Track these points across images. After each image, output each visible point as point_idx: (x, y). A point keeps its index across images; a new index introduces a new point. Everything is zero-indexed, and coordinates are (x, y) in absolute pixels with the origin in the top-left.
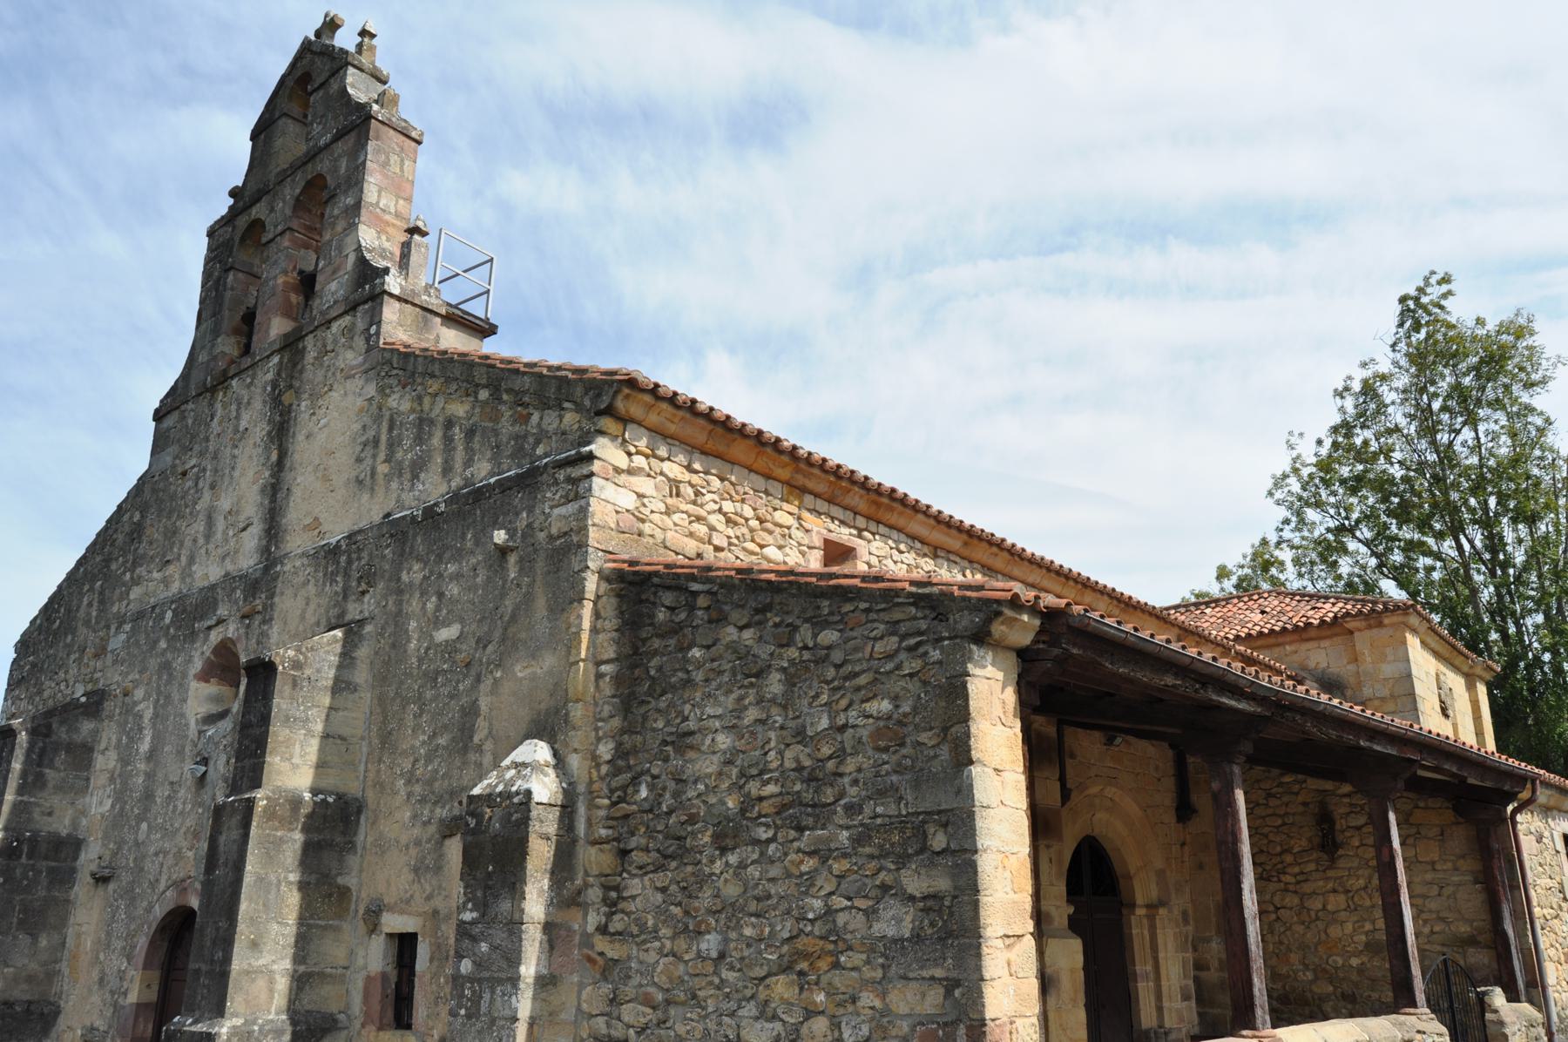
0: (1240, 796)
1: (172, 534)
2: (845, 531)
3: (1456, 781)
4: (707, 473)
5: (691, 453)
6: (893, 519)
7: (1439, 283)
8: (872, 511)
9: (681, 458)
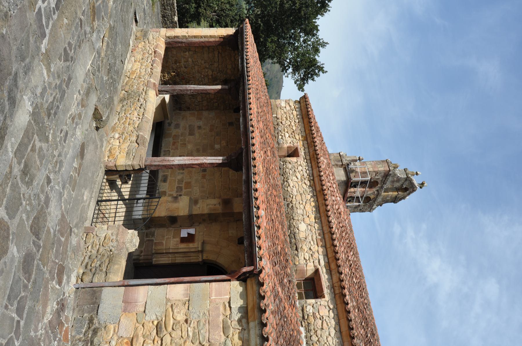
0: (219, 87)
2: (303, 154)
3: (346, 302)
4: (298, 119)
5: (300, 115)
6: (313, 163)
7: (39, 206)
8: (312, 156)
9: (298, 113)
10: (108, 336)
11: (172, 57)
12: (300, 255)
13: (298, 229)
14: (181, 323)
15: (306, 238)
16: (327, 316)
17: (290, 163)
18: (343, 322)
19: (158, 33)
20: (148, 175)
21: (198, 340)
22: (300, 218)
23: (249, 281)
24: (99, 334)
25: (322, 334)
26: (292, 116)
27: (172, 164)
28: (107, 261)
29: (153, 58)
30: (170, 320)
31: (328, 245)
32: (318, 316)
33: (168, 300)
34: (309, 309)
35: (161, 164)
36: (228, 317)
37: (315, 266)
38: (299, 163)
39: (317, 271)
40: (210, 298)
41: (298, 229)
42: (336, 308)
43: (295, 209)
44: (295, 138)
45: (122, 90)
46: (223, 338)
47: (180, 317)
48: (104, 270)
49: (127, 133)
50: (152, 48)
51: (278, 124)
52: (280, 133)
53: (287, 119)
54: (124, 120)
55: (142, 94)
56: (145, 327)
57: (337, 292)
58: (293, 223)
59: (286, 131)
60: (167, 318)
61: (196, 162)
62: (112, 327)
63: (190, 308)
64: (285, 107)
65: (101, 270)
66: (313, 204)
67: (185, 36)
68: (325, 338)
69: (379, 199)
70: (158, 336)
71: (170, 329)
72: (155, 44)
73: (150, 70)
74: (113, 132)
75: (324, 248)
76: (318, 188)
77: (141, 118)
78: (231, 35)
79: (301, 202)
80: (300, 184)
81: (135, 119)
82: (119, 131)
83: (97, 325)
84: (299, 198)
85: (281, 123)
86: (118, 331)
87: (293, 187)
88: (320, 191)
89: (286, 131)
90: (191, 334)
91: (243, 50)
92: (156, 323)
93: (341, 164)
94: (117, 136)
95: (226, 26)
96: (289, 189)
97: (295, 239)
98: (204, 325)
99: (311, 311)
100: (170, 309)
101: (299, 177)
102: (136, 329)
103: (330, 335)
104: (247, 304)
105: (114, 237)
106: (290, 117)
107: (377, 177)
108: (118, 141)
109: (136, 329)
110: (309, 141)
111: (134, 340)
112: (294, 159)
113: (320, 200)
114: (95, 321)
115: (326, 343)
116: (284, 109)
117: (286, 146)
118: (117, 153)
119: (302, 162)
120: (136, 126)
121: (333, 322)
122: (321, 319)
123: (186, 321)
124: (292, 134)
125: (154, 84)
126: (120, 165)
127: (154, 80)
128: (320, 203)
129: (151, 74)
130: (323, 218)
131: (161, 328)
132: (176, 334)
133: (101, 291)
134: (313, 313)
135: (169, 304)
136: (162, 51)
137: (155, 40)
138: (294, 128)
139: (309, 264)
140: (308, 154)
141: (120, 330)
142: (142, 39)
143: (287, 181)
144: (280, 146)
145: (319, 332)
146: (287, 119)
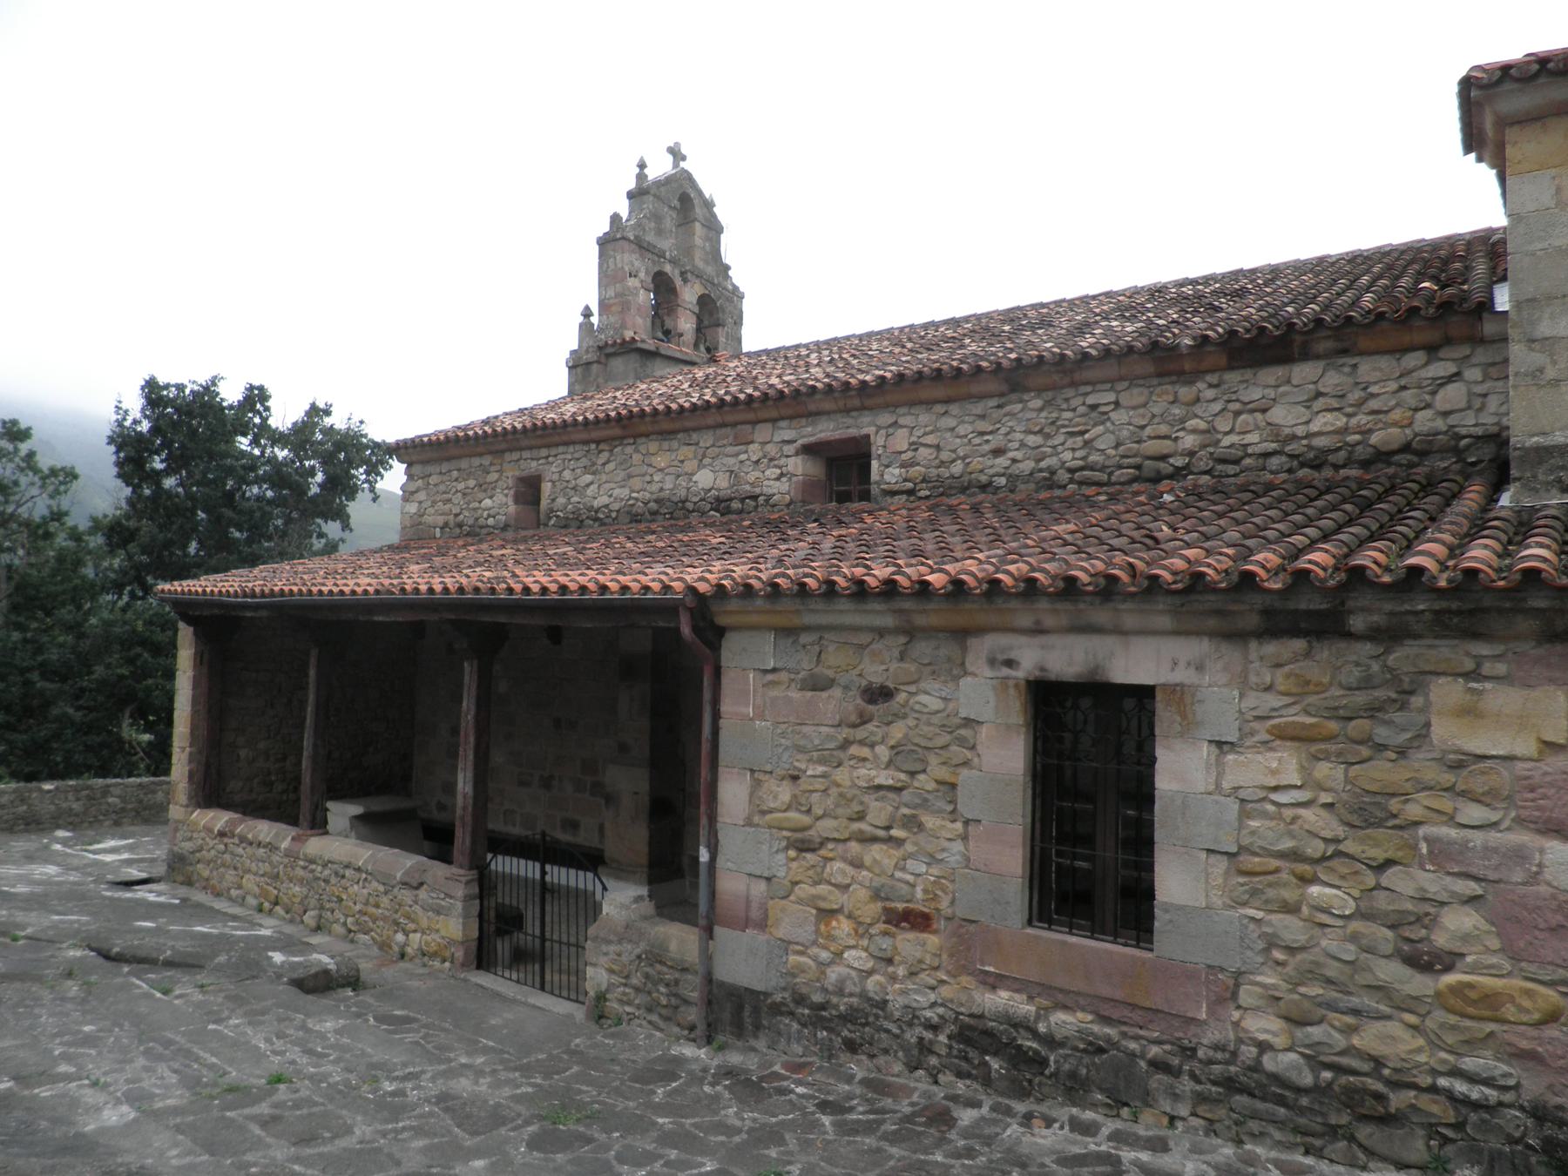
1: (840, 992)
8: (539, 442)
10: (810, 968)
11: (251, 791)
12: (770, 491)
13: (710, 490)
14: (797, 792)
15: (732, 472)
16: (911, 434)
17: (553, 500)
18: (926, 392)
19: (180, 826)
20: (500, 858)
21: (835, 753)
22: (684, 484)
23: (722, 620)
24: (804, 990)
25: (949, 447)
26: (442, 488)
27: (471, 801)
28: (658, 967)
29: (236, 841)
30: (787, 819)
31: (751, 416)
32: (910, 454)
33: (749, 823)
34: (893, 475)
35: (469, 829)
36: (792, 676)
37: (797, 454)
38: (555, 477)
39: (809, 450)
40: (751, 719)
41: (710, 490)
42: (892, 406)
43: (662, 494)
44: (496, 481)
45: (302, 922)
46: (837, 692)
47: (785, 793)
48: (677, 975)
49: (396, 912)
50: (211, 843)
51: (460, 525)
52: (482, 521)
53: (449, 500)
54: (366, 918)
55: (312, 871)
56: (798, 879)
57: (857, 402)
58: (695, 503)
59: (477, 505)
60: (786, 825)
61: (472, 739)
62: (793, 958)
63: (768, 768)
64: (420, 502)
65: (677, 982)
66: (653, 446)
67: (191, 754)
68: (958, 440)
69: (710, 270)
70: (819, 848)
71: (806, 820)
72: (202, 834)
73: (262, 850)
74: (391, 948)
75: (759, 426)
76: (617, 431)
77: (364, 876)
78: (196, 634)
79: (648, 478)
80: (604, 477)
81: (365, 891)
82: (391, 933)
83: (786, 995)
84: (637, 483)
85: (456, 515)
86: (802, 945)
87: (611, 496)
88: (624, 427)
89: (477, 505)
90: (820, 769)
91: (222, 605)
92: (792, 853)
93: (595, 366)
94: (400, 937)
95: (173, 645)
96: (616, 506)
97: (731, 499)
98: (805, 736)
99: (897, 471)
100: (768, 817)
101: (588, 478)
102: (800, 901)
103: (953, 429)
104: (770, 628)
105: (612, 948)
106: (444, 493)
107: (642, 275)
108: (411, 935)
109: (800, 901)
110: (504, 446)
111: (823, 905)
112: (546, 488)
113: (643, 429)
114: (778, 998)
115: (970, 441)
116: (424, 505)
117: (512, 508)
118: (436, 937)
119: (554, 469)
120: (381, 888)
121: (924, 418)
122: (916, 450)
123: (795, 778)
124: (485, 491)
125: (293, 839)
126: (464, 930)
127: (284, 839)
128: (650, 429)
129: (272, 847)
130: (688, 424)
131: (803, 841)
132: (819, 804)
133: (722, 984)
134: (902, 466)
135: (756, 819)
136: (220, 819)
137: (195, 835)
138: (472, 483)
139: (790, 468)
140: (535, 453)
141: (800, 940)
142: (191, 869)
143: (596, 512)
144: (513, 522)
145: (945, 456)
146: (449, 500)
